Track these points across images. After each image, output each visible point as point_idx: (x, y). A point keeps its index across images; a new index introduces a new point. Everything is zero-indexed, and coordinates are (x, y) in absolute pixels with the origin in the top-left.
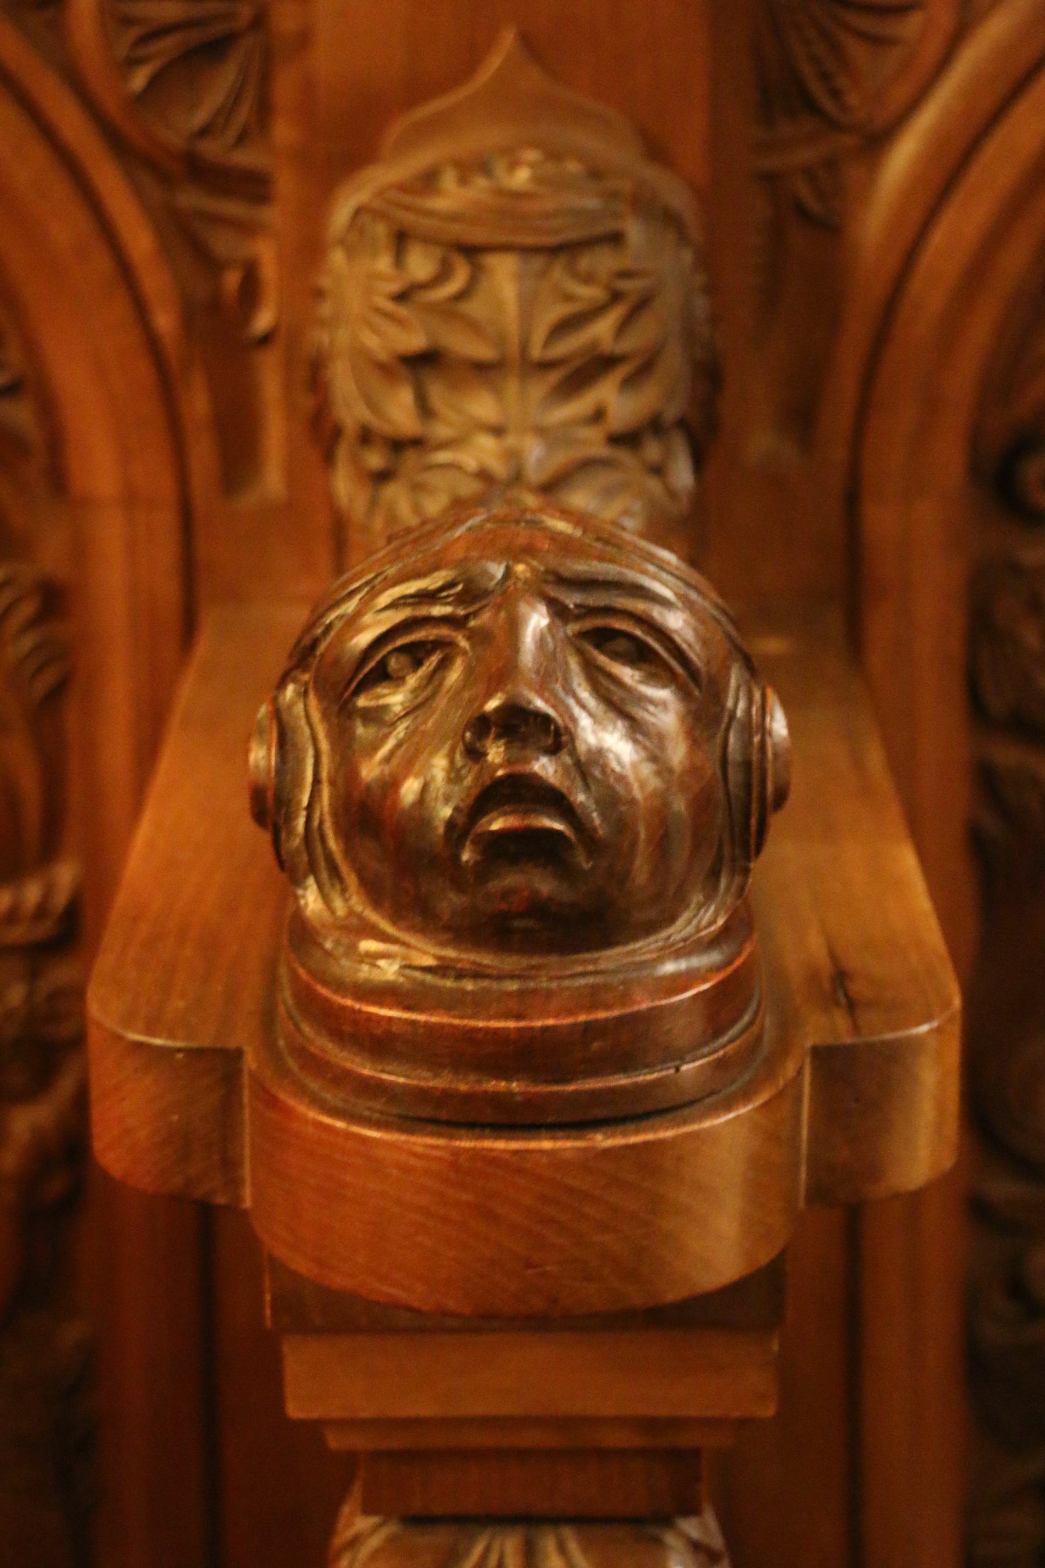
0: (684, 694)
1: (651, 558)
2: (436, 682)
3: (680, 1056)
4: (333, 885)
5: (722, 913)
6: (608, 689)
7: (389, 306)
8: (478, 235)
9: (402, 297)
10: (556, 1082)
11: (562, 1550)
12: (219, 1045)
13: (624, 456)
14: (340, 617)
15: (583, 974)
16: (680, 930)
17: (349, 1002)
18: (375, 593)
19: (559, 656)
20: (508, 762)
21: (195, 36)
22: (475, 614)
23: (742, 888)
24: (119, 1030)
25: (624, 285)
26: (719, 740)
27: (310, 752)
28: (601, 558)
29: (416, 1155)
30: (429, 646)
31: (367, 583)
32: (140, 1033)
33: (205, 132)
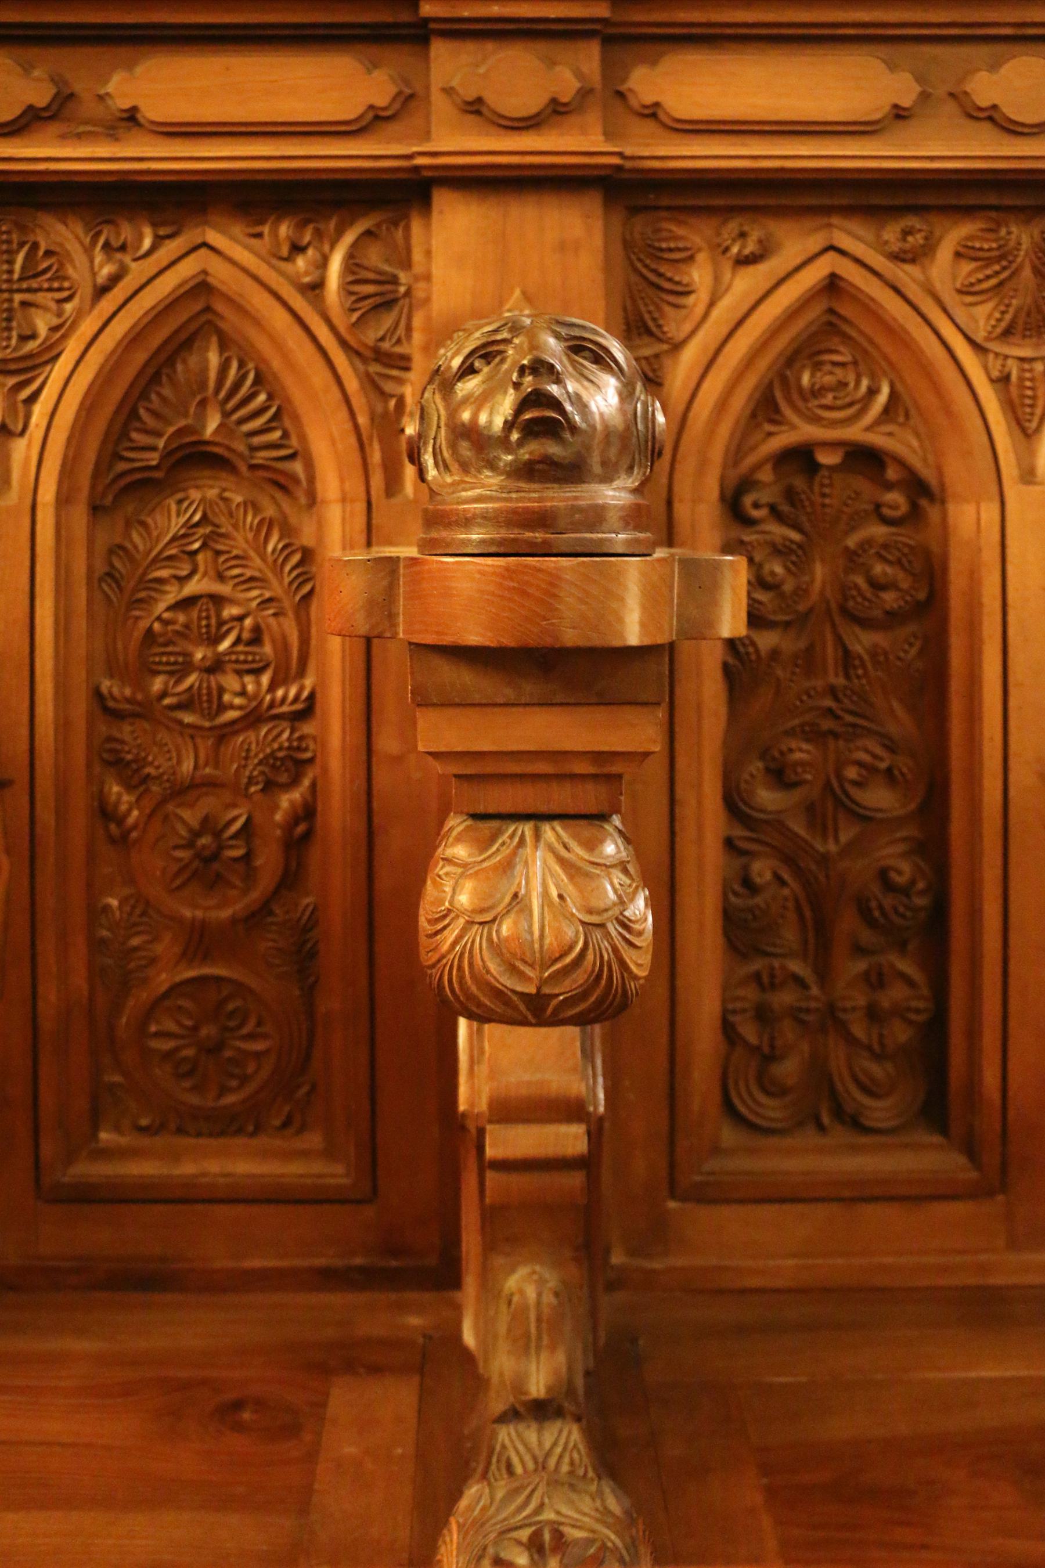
11: (553, 829)
16: (617, 483)
21: (379, 300)
33: (382, 339)
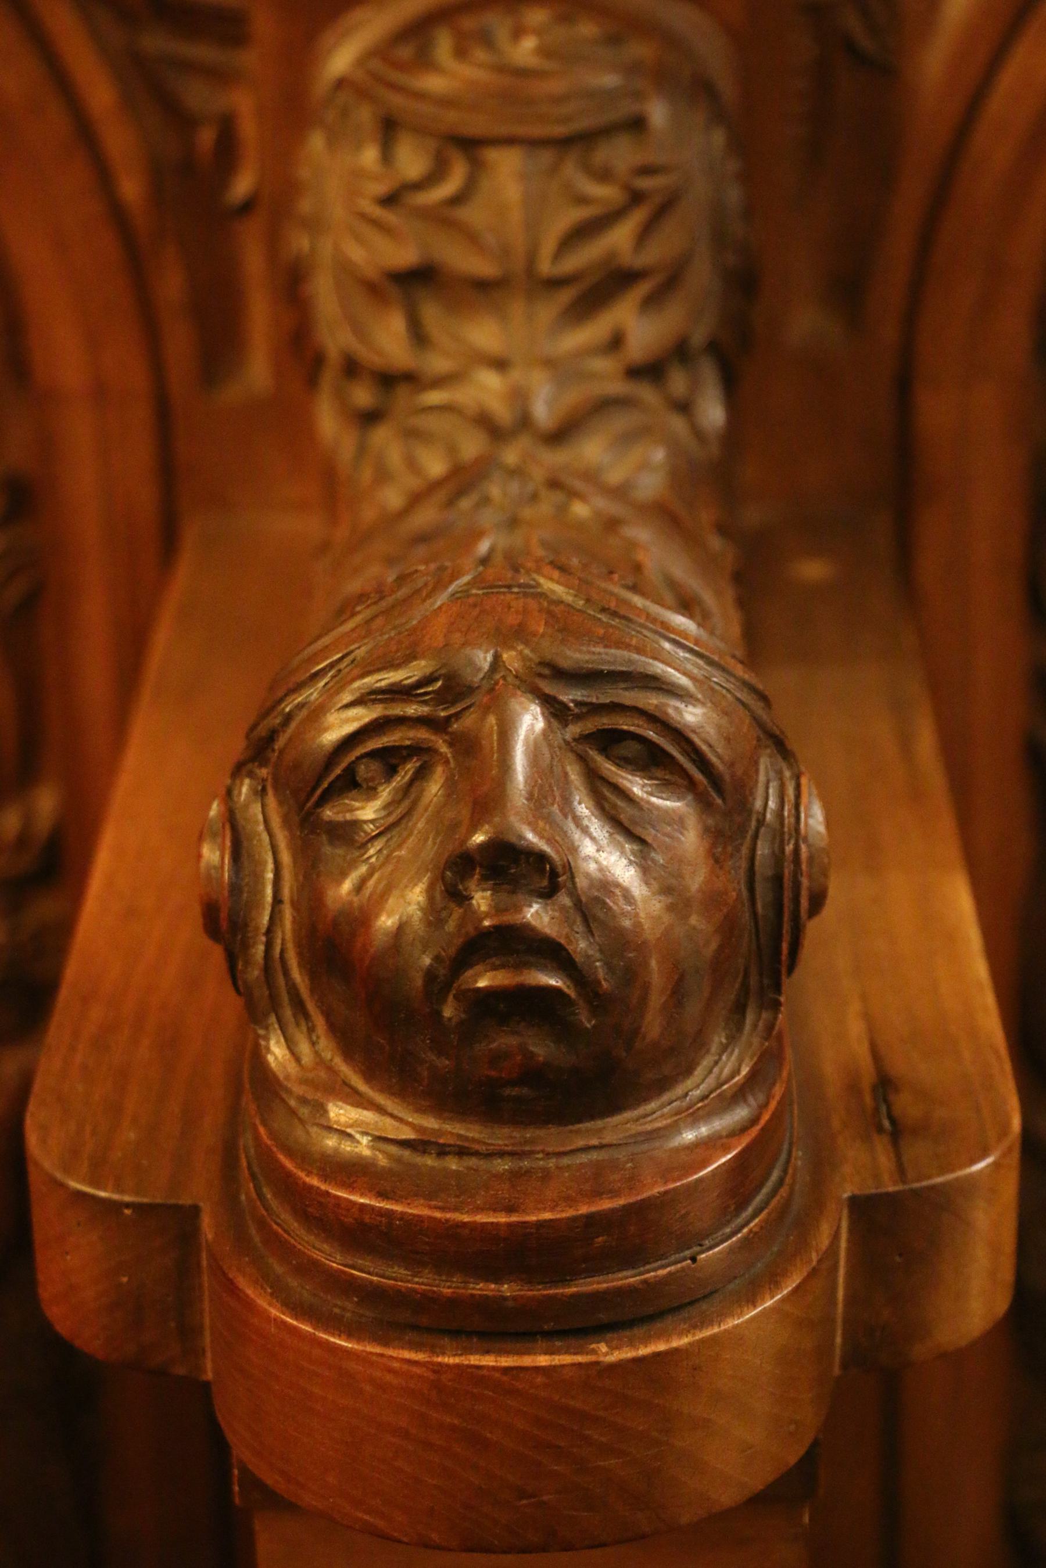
0: (704, 803)
1: (666, 630)
2: (413, 796)
3: (698, 1239)
4: (298, 1025)
5: (747, 1060)
6: (615, 806)
7: (378, 212)
8: (476, 125)
9: (390, 200)
10: (554, 1283)
12: (172, 1201)
13: (647, 393)
14: (301, 706)
15: (587, 1149)
17: (315, 1181)
18: (341, 686)
19: (558, 770)
20: (498, 909)
22: (457, 716)
23: (770, 1027)
24: (59, 1175)
25: (644, 183)
26: (745, 851)
27: (270, 866)
28: (607, 641)
29: (390, 1370)
30: (405, 753)
31: (331, 666)
32: (83, 1181)
